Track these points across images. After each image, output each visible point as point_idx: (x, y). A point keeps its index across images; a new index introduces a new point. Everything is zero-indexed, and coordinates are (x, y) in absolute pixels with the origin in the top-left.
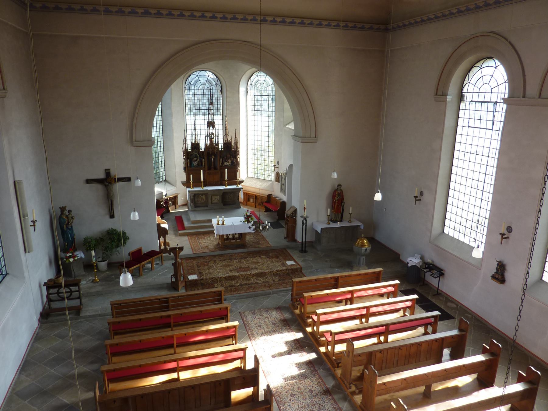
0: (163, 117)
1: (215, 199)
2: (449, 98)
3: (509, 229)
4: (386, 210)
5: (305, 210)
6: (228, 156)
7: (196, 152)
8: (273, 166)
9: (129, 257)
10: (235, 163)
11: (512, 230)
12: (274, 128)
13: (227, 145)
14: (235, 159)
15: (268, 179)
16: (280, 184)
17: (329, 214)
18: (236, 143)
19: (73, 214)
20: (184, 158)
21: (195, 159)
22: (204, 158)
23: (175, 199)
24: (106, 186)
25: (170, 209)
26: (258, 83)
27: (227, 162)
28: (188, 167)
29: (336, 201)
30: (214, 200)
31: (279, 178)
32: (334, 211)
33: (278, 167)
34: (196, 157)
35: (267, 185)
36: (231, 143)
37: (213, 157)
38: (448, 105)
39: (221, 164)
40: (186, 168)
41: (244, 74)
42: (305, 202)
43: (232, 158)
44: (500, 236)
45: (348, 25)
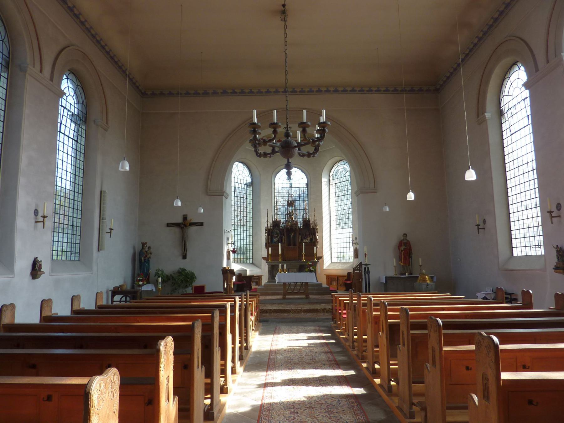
2: (488, 115)
3: (559, 207)
4: (460, 260)
5: (366, 256)
6: (308, 233)
7: (277, 230)
8: (350, 241)
9: (192, 291)
10: (314, 241)
11: (561, 207)
13: (306, 223)
15: (350, 261)
17: (395, 265)
19: (152, 250)
21: (276, 235)
22: (284, 235)
24: (182, 228)
26: (338, 172)
27: (306, 239)
28: (269, 244)
29: (402, 251)
32: (401, 262)
34: (277, 234)
36: (309, 221)
37: (293, 234)
38: (489, 123)
39: (300, 241)
40: (267, 245)
41: (325, 165)
42: (366, 248)
43: (311, 236)
44: (549, 214)
45: (397, 88)
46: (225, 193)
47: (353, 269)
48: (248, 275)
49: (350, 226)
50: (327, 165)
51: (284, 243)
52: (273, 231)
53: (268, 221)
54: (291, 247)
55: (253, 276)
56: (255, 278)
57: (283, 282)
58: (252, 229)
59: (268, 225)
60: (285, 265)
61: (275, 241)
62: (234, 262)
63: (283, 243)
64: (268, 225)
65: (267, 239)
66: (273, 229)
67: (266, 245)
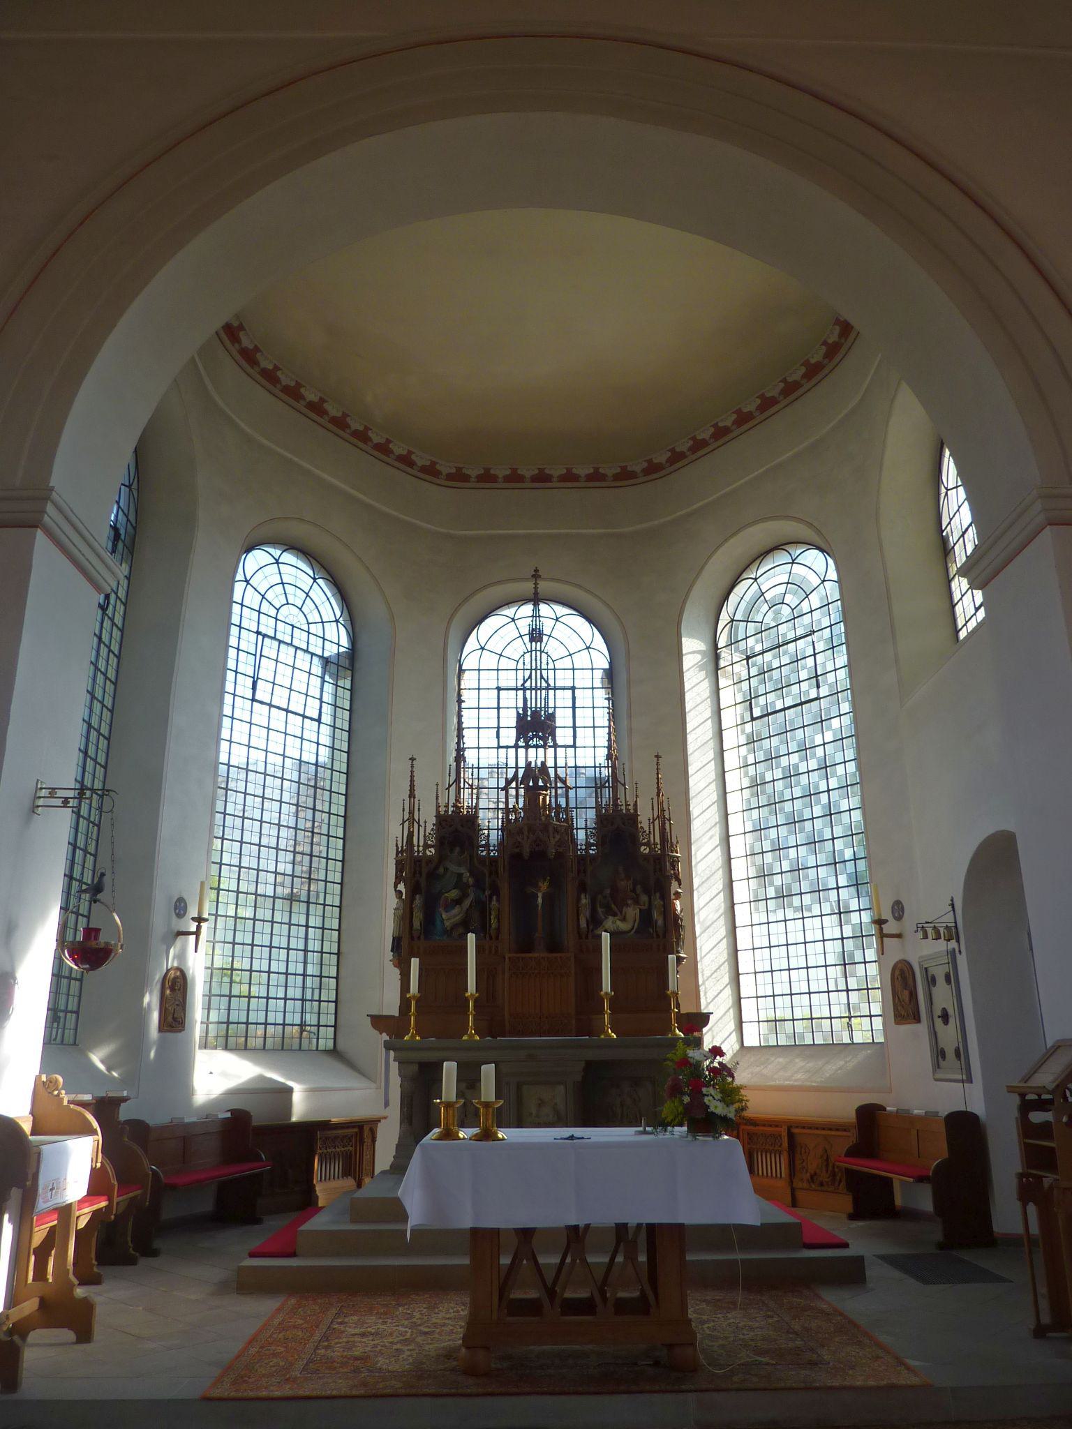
0: (353, 758)
1: (541, 1103)
7: (460, 865)
10: (660, 922)
12: (851, 767)
14: (658, 902)
15: (852, 1038)
16: (922, 1028)
18: (662, 819)
20: (399, 893)
21: (454, 894)
22: (495, 891)
23: (362, 1142)
25: (318, 1193)
27: (614, 915)
28: (412, 938)
30: (534, 1112)
31: (913, 995)
33: (899, 936)
34: (459, 884)
35: (850, 1065)
36: (633, 818)
39: (583, 924)
43: (644, 898)
46: (50, 508)
47: (1016, 1100)
48: (294, 1119)
49: (841, 852)
50: (706, 574)
51: (497, 938)
52: (441, 870)
53: (411, 819)
54: (536, 955)
55: (324, 1125)
56: (336, 1137)
57: (467, 1222)
58: (343, 873)
59: (411, 835)
60: (488, 1071)
61: (447, 924)
62: (222, 1041)
63: (493, 933)
64: (411, 835)
65: (405, 916)
66: (441, 857)
67: (397, 945)
